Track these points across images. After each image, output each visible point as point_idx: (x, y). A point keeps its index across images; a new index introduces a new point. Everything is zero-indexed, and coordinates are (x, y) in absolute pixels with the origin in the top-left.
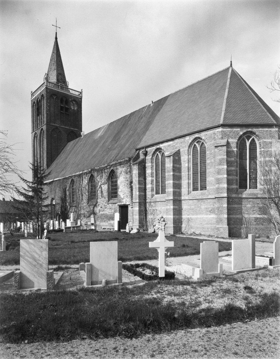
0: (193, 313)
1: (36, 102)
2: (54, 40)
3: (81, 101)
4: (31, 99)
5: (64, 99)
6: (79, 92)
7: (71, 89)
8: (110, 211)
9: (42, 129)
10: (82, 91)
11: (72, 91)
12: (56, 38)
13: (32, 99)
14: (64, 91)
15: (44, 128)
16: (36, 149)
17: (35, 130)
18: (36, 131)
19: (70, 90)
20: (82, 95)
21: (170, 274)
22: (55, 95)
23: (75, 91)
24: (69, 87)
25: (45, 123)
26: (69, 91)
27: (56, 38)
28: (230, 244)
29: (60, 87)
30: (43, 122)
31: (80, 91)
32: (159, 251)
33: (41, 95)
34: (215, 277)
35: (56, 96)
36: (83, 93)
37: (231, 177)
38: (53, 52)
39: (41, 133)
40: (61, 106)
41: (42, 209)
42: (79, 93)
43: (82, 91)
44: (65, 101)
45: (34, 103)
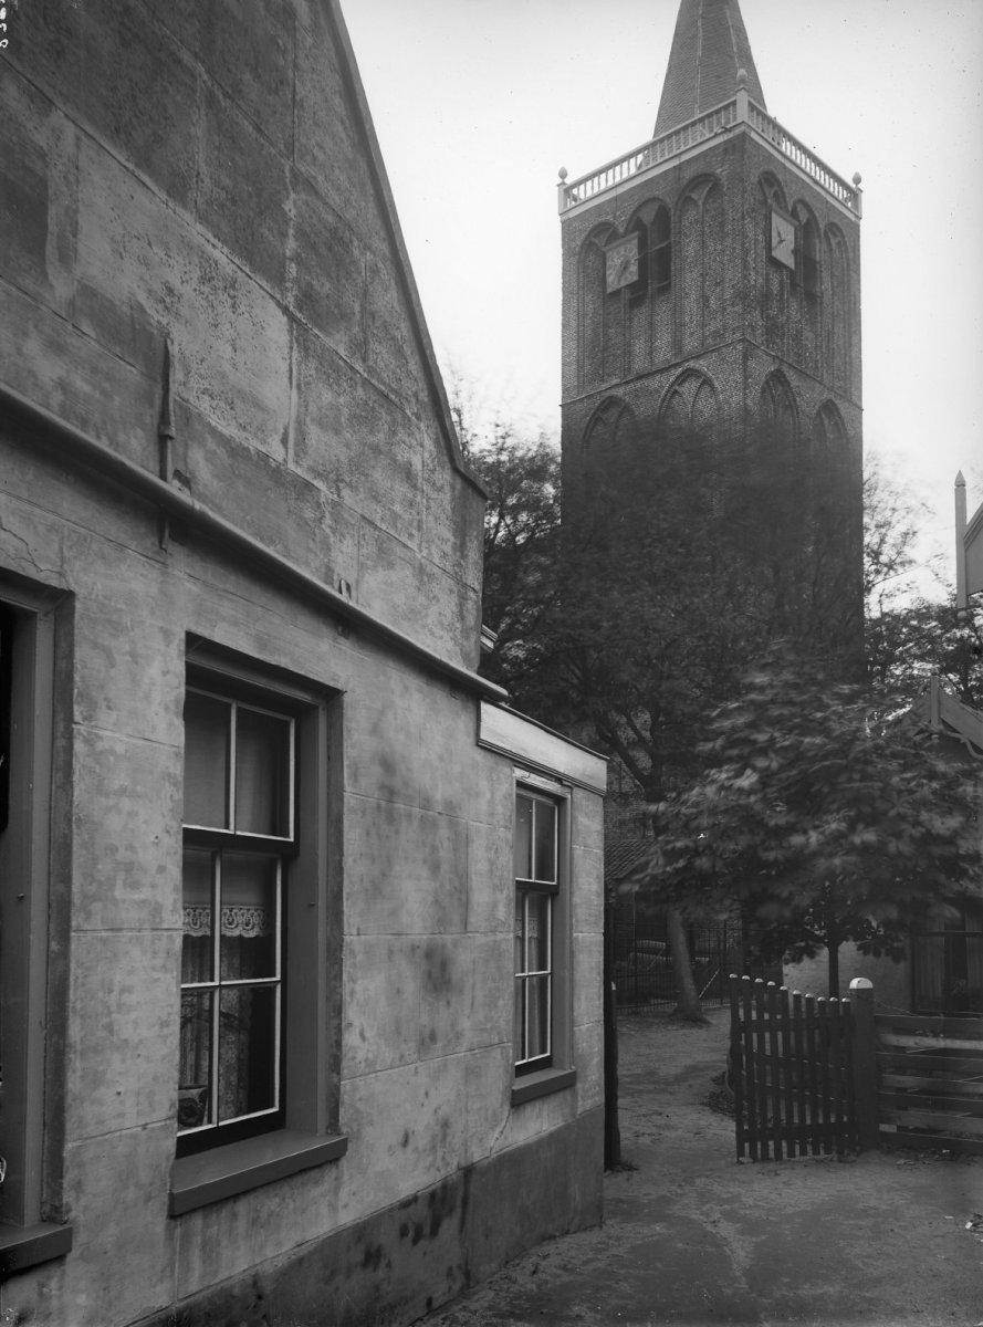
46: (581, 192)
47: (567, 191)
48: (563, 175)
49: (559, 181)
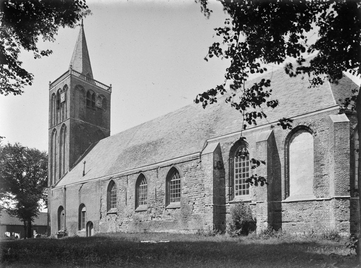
0: (226, 227)
4: (49, 90)
5: (92, 93)
7: (98, 82)
9: (64, 124)
10: (111, 86)
11: (102, 86)
13: (51, 90)
15: (67, 123)
16: (54, 148)
17: (53, 126)
18: (55, 128)
20: (111, 90)
21: (200, 242)
22: (80, 86)
24: (94, 78)
25: (68, 117)
26: (95, 84)
28: (236, 169)
30: (65, 116)
31: (110, 86)
32: (327, 13)
33: (64, 85)
37: (283, 147)
38: (77, 46)
39: (62, 129)
42: (108, 88)
44: (92, 94)
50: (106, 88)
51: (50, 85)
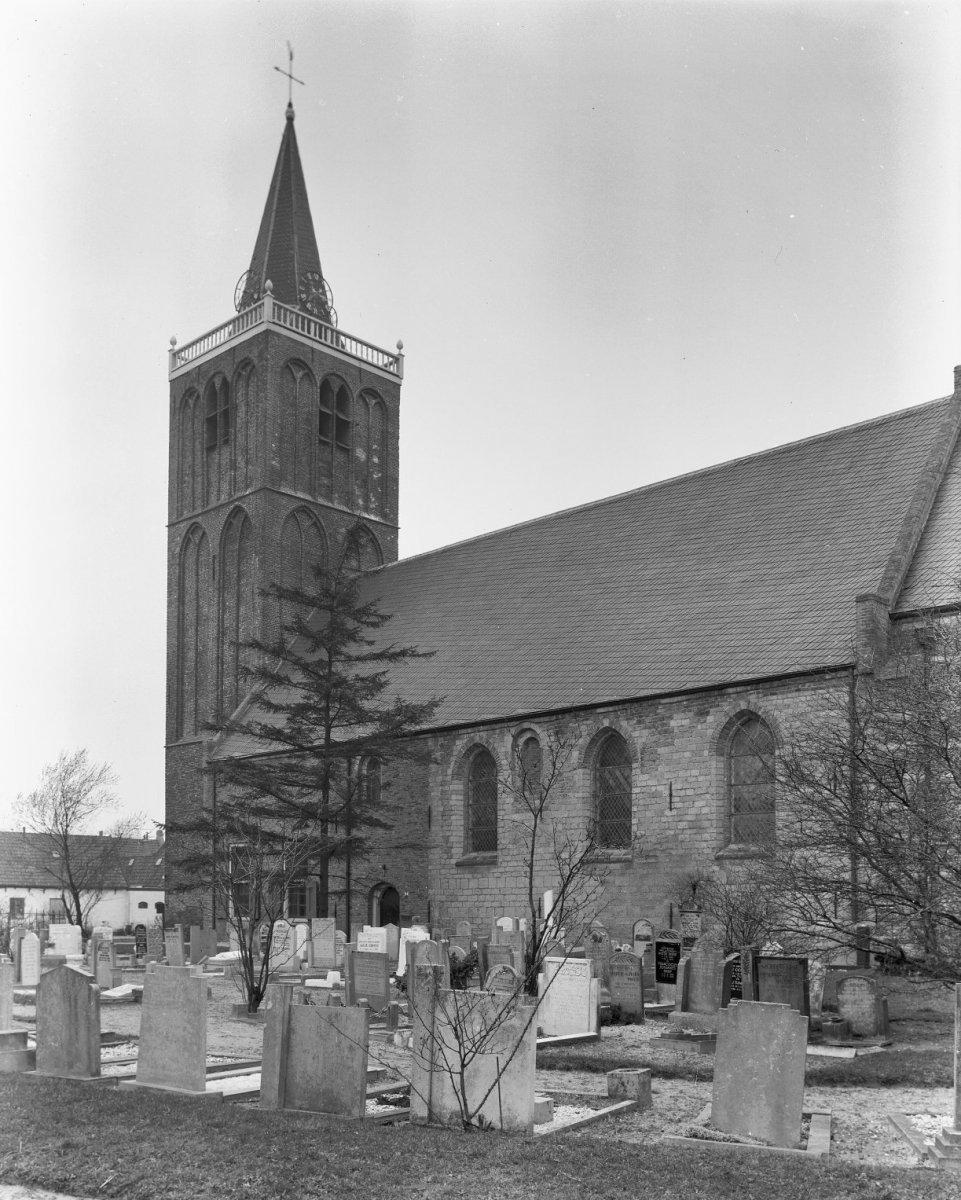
1: (201, 390)
2: (284, 122)
3: (397, 398)
6: (392, 356)
8: (342, 953)
10: (403, 352)
12: (290, 119)
14: (317, 338)
19: (348, 340)
23: (380, 354)
24: (340, 328)
27: (290, 119)
29: (313, 325)
31: (395, 352)
34: (771, 1155)
35: (376, 398)
36: (406, 363)
40: (321, 412)
41: (363, 1107)
42: (391, 359)
43: (403, 352)
44: (336, 390)
45: (190, 392)
46: (189, 354)
47: (175, 355)
48: (173, 343)
49: (171, 347)
50: (380, 360)
51: (174, 355)
